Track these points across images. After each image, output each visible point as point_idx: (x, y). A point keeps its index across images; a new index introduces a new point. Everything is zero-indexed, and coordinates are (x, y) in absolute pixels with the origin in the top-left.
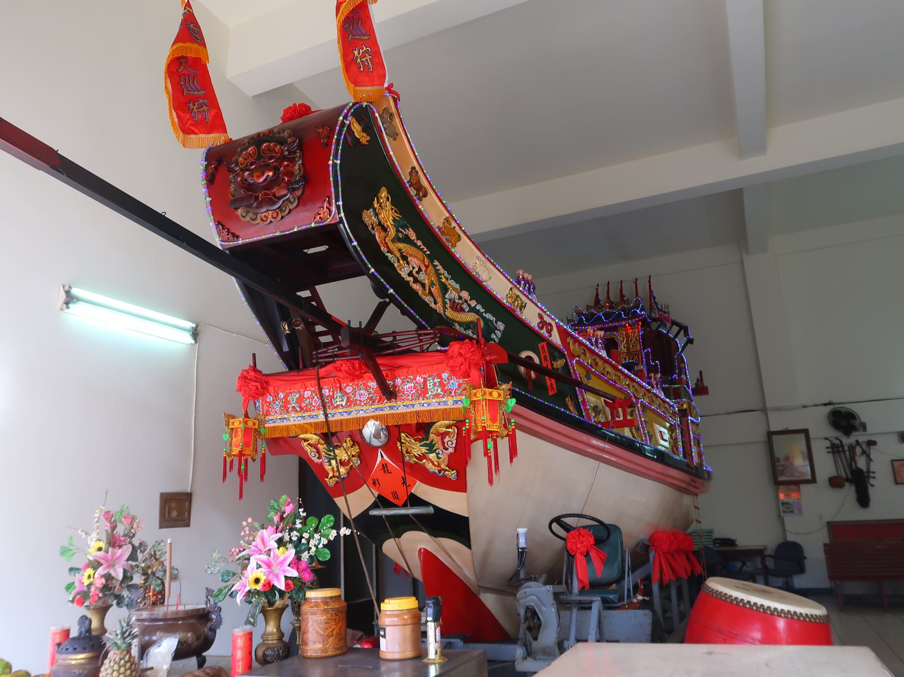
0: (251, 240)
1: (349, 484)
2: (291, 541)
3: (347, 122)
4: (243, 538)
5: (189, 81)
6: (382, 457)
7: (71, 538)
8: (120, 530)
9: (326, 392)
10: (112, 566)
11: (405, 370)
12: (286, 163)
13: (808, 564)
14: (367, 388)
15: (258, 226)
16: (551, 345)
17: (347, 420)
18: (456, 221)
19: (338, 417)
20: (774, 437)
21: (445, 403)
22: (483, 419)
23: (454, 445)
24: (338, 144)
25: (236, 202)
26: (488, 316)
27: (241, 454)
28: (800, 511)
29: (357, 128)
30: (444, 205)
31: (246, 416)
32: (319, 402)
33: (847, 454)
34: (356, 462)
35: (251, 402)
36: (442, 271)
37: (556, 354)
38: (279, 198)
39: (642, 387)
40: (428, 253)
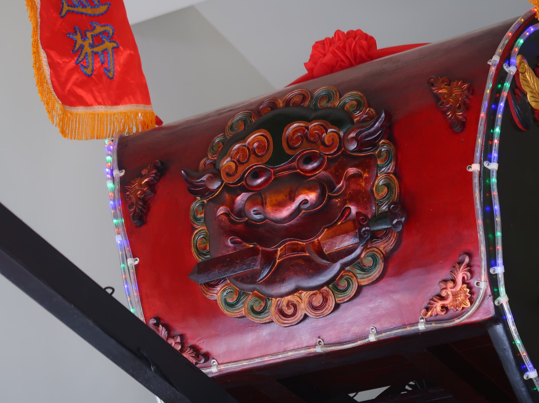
3: (512, 70)
12: (352, 171)
24: (491, 124)
38: (335, 257)
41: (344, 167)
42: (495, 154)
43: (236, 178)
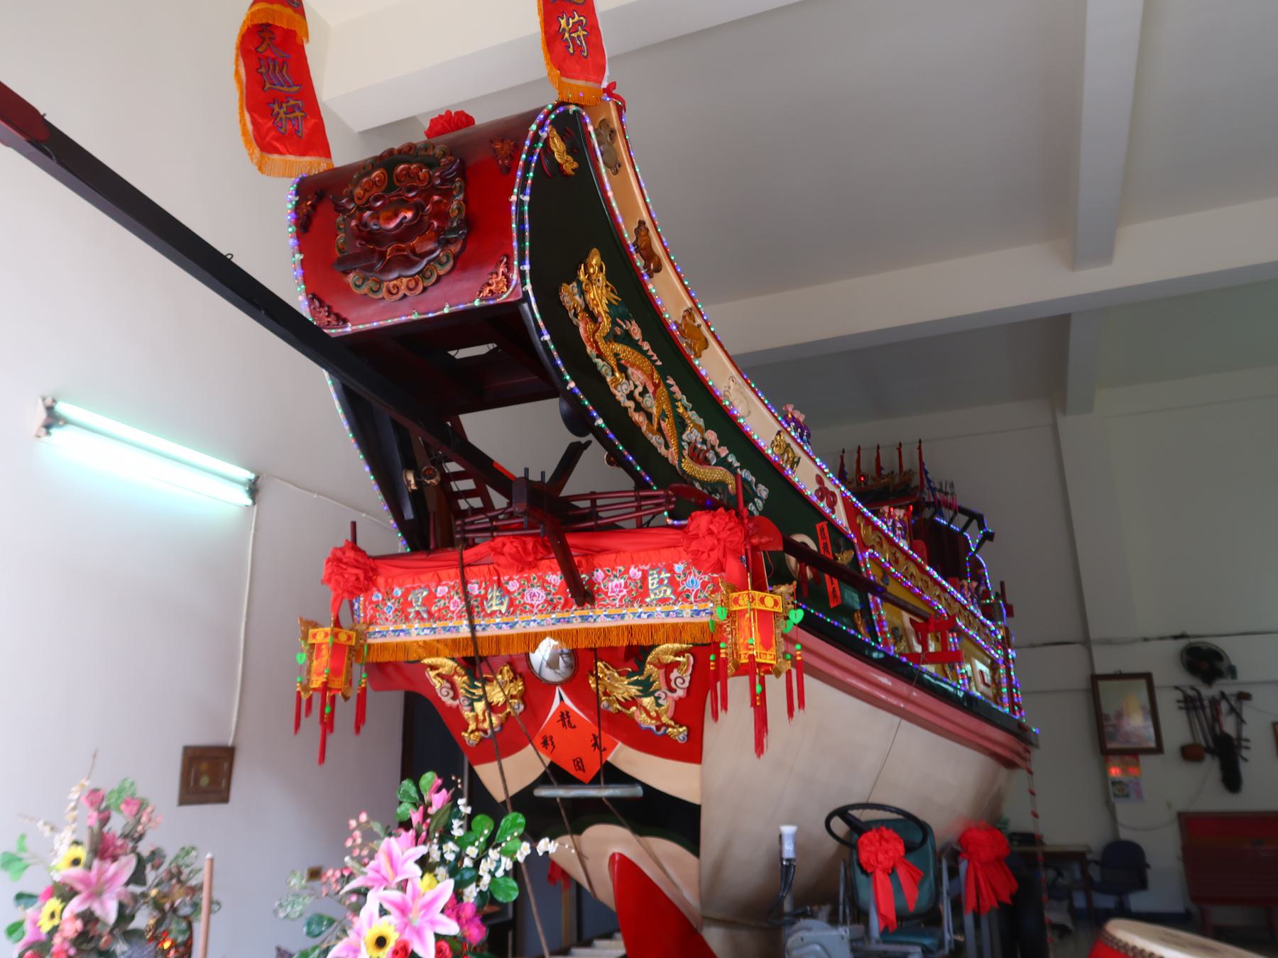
0: (368, 326)
1: (501, 744)
2: (443, 861)
3: (544, 135)
4: (349, 851)
5: (274, 65)
6: (560, 700)
7: (23, 837)
8: (117, 825)
9: (474, 588)
10: (96, 894)
11: (613, 556)
12: (436, 198)
13: (1151, 875)
14: (544, 584)
15: (382, 304)
16: (833, 526)
17: (508, 637)
18: (702, 316)
19: (492, 631)
20: (1102, 685)
21: (678, 614)
22: (749, 644)
23: (687, 684)
24: (526, 169)
25: (347, 262)
26: (745, 473)
27: (325, 687)
28: (1139, 795)
29: (558, 146)
30: (685, 287)
31: (337, 623)
32: (462, 605)
33: (1208, 711)
34: (518, 707)
35: (346, 602)
36: (679, 395)
37: (841, 542)
38: (423, 256)
39: (957, 600)
40: (659, 363)
41: (431, 196)
42: (528, 191)
43: (364, 201)
